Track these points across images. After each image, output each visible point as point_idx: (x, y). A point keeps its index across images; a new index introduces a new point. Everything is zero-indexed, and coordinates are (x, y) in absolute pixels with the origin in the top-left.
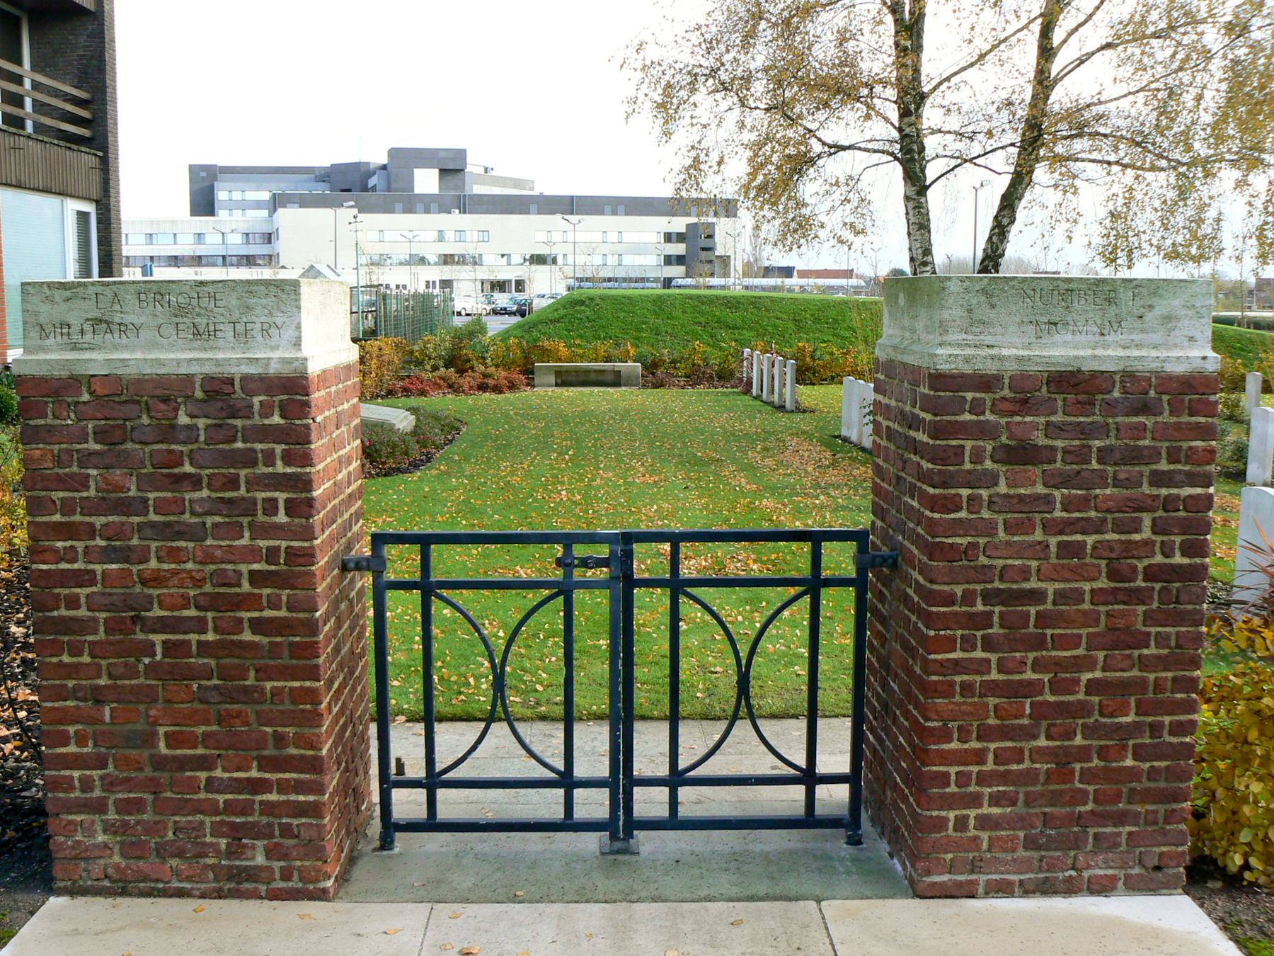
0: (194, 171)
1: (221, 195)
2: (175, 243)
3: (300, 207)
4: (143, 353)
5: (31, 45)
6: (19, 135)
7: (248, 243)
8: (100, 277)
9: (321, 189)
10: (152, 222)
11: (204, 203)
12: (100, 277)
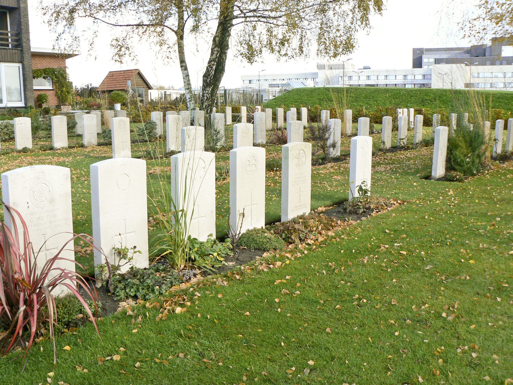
0: (415, 51)
1: (425, 60)
2: (396, 79)
3: (446, 64)
4: (455, 120)
5: (9, 17)
6: (7, 49)
7: (424, 79)
8: (465, 88)
9: (467, 56)
10: (387, 71)
11: (418, 63)
12: (465, 88)
